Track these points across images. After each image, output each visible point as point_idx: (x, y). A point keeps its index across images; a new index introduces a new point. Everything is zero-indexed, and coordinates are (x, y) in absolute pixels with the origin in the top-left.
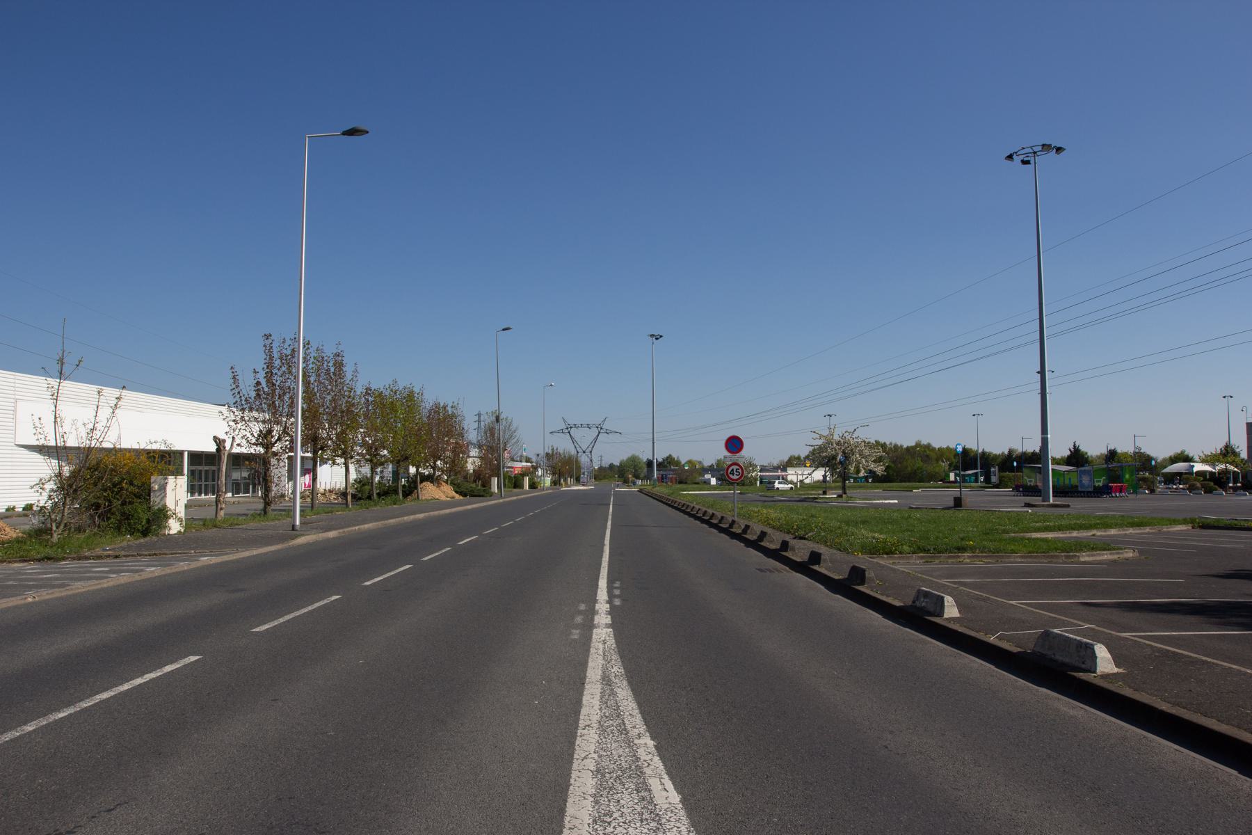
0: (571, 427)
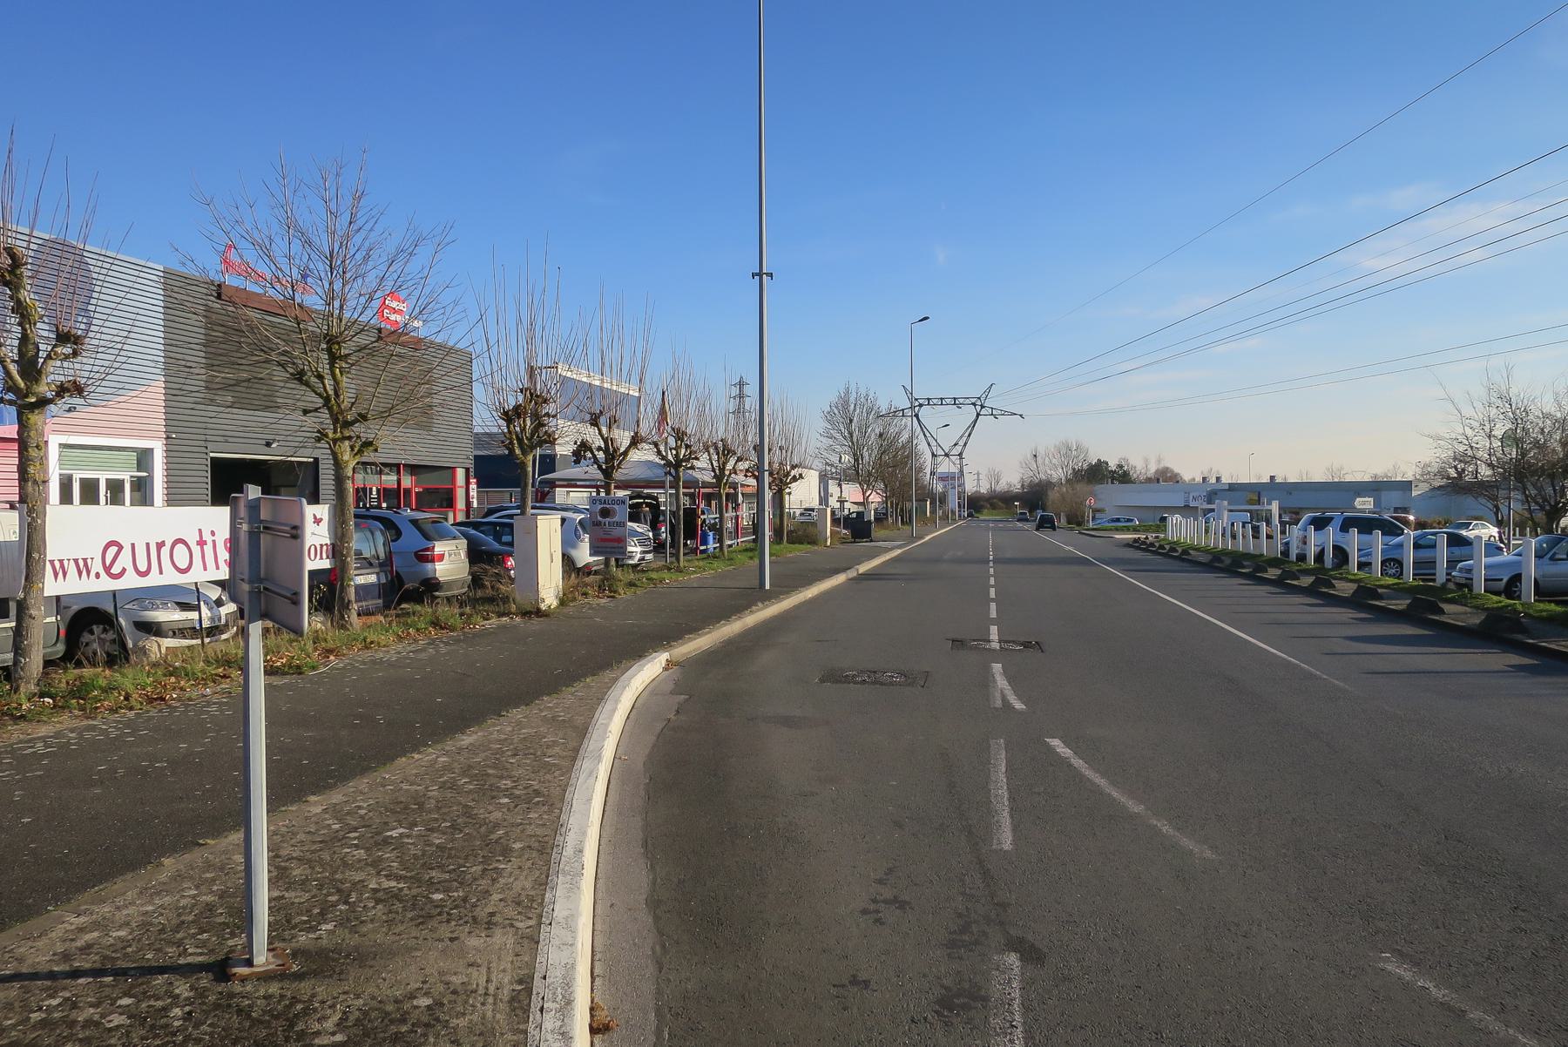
0: (921, 405)
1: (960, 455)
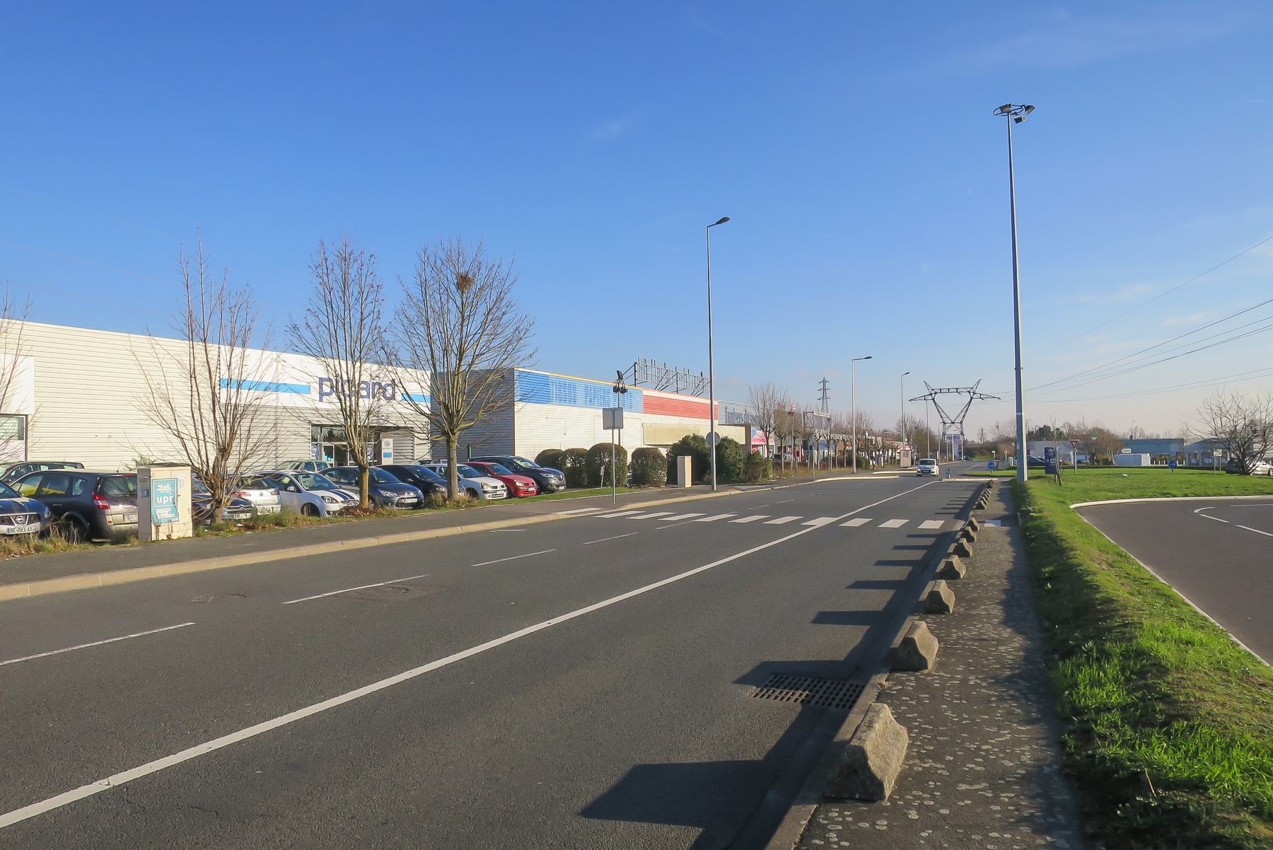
0: (936, 393)
1: (961, 423)
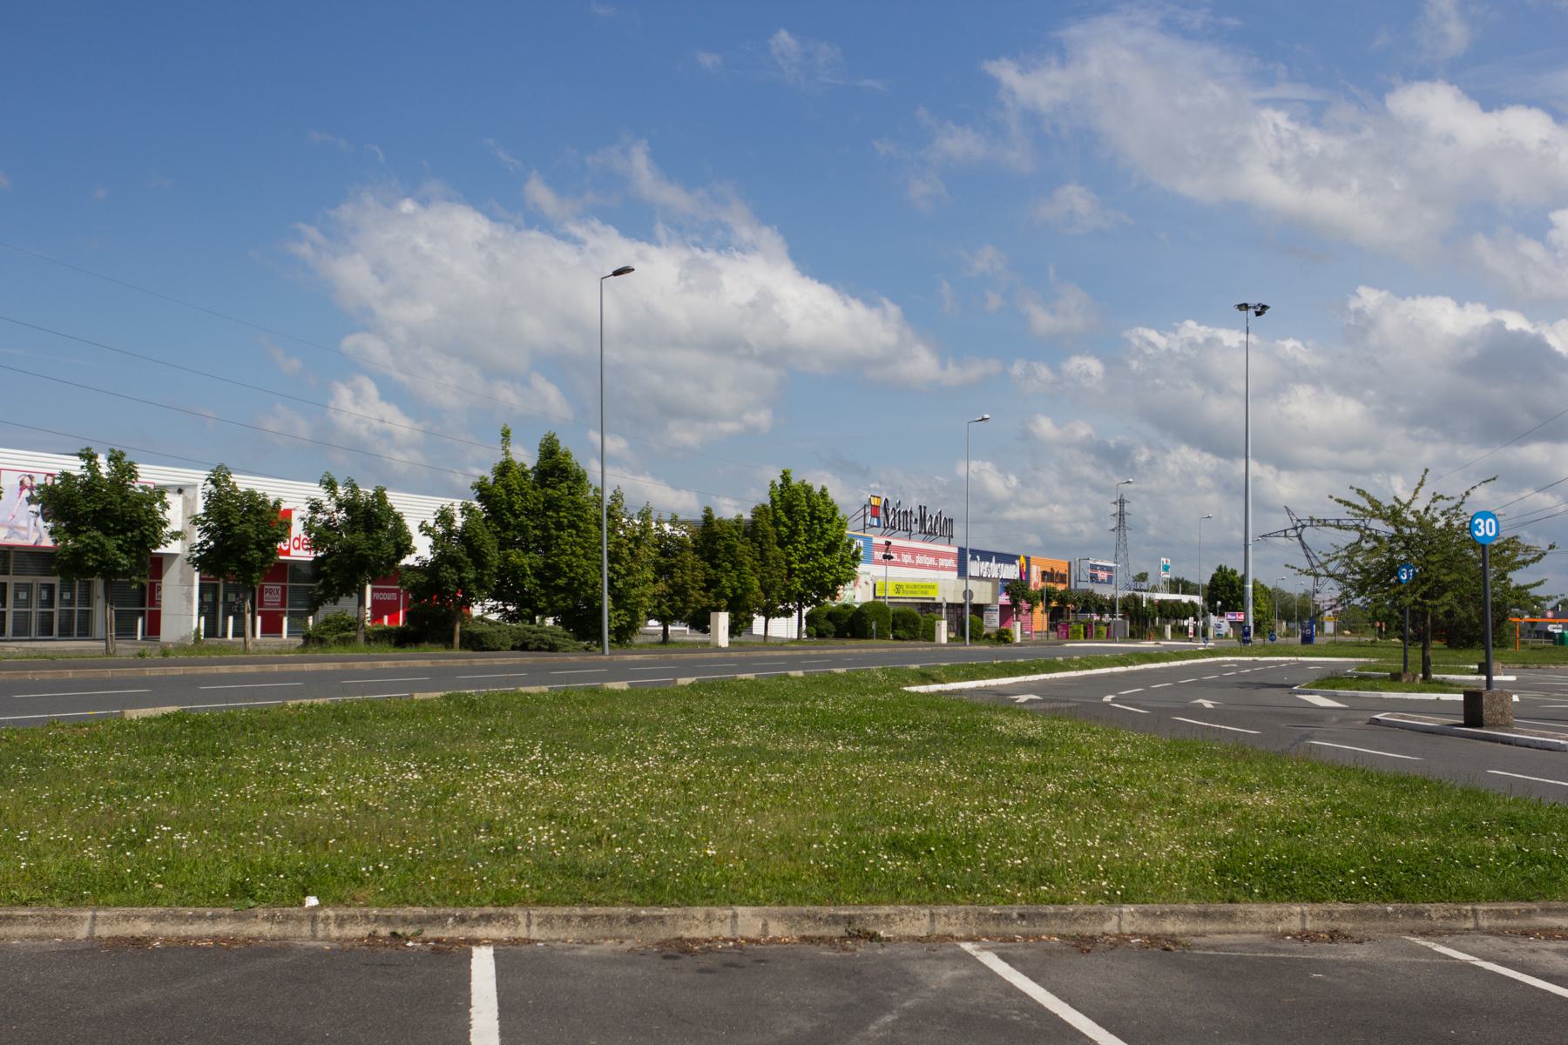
0: (1303, 526)
